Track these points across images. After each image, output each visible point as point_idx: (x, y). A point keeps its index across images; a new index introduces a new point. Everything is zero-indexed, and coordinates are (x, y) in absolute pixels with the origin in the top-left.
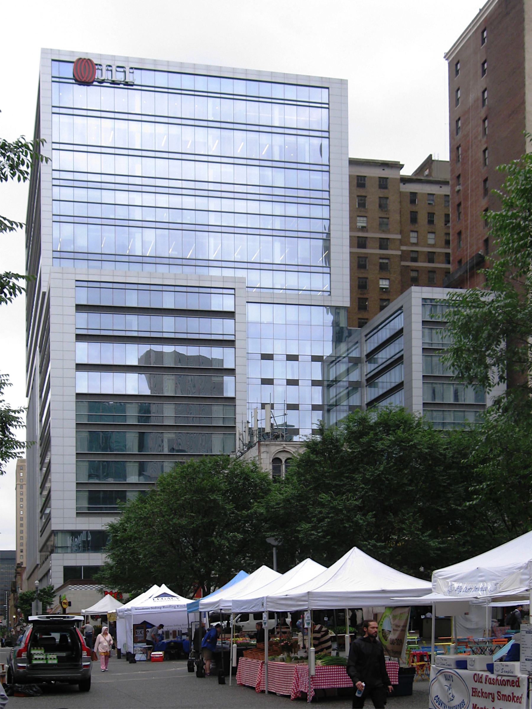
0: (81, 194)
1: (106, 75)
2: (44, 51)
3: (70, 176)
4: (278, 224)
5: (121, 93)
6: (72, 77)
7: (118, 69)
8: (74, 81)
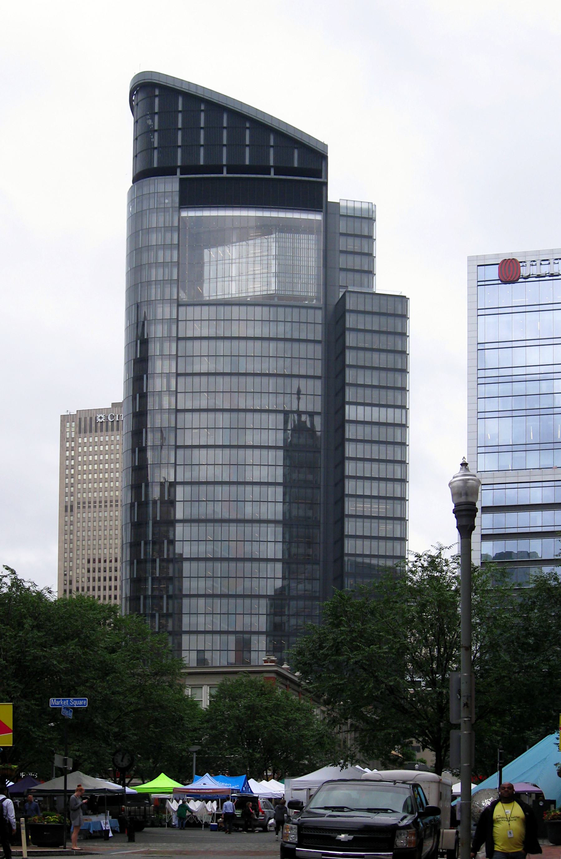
0: (505, 389)
1: (534, 270)
2: (470, 259)
3: (494, 373)
4: (509, 404)
5: (546, 285)
6: (498, 278)
7: (543, 263)
8: (500, 282)
